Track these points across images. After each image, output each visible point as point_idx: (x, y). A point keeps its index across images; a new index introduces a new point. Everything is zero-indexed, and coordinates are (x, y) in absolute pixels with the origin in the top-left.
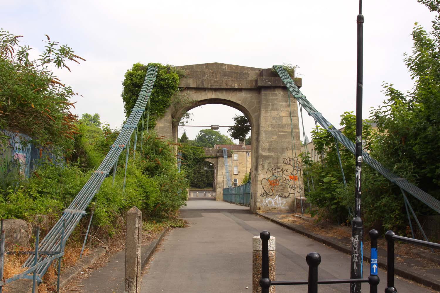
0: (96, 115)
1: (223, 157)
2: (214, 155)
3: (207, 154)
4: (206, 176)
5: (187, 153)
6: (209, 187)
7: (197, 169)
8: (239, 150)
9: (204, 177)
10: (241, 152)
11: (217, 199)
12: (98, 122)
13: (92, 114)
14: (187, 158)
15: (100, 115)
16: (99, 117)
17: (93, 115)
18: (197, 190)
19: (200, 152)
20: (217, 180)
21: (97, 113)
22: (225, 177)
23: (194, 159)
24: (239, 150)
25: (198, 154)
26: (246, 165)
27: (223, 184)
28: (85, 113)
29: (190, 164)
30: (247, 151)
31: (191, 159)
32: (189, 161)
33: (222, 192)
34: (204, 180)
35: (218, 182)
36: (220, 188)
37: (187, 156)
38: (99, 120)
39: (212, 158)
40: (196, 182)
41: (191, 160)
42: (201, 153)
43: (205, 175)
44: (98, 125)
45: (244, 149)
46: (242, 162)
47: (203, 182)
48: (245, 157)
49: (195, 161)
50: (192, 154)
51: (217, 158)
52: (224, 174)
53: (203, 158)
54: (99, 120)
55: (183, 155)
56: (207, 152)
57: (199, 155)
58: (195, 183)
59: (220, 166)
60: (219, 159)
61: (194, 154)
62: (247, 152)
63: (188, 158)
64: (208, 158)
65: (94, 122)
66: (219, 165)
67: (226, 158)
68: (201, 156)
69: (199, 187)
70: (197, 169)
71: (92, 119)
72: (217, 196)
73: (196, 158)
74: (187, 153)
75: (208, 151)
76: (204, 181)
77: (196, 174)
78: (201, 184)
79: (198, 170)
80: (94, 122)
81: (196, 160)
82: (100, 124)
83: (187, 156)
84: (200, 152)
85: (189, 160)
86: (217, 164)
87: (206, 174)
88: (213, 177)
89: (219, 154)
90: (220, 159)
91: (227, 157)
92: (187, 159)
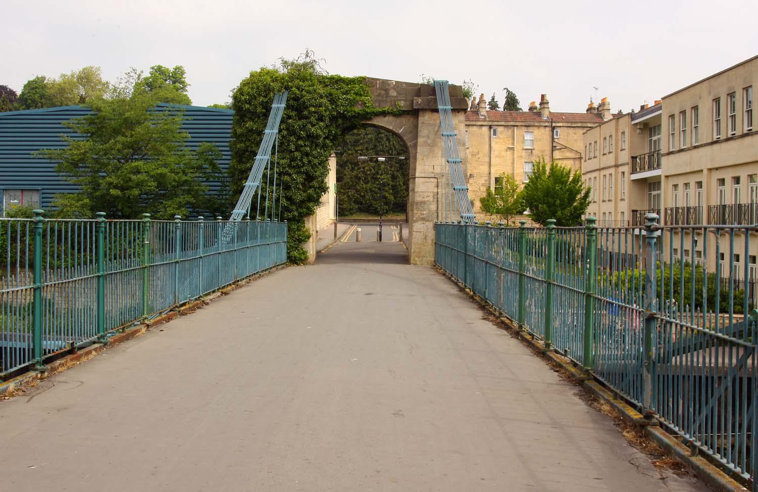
0: (179, 68)
1: (436, 111)
2: (402, 103)
3: (380, 102)
4: (392, 186)
5: (308, 96)
6: (398, 212)
7: (371, 170)
8: (474, 123)
9: (386, 188)
10: (475, 128)
11: (413, 258)
12: (183, 83)
13: (170, 66)
14: (306, 113)
15: (186, 69)
16: (183, 73)
17: (172, 70)
18: (370, 218)
19: (356, 94)
20: (414, 190)
21: (179, 65)
22: (443, 181)
23: (333, 119)
24: (474, 123)
25: (347, 99)
26: (487, 159)
27: (433, 207)
28: (156, 64)
29: (318, 137)
30: (490, 123)
31: (321, 119)
32: (313, 125)
33: (431, 234)
34: (387, 195)
35: (418, 199)
36: (423, 219)
37: (306, 108)
38: (184, 78)
39: (399, 114)
40: (369, 200)
41: (322, 121)
42: (358, 98)
43: (389, 185)
44: (182, 88)
45: (485, 120)
46: (478, 153)
47: (384, 200)
48: (487, 139)
49: (338, 126)
50: (324, 101)
51: (414, 113)
52: (438, 170)
53: (367, 116)
54: (184, 78)
55: (291, 102)
56: (379, 95)
57: (352, 103)
58: (366, 204)
59: (426, 144)
60: (421, 119)
61: (333, 101)
62: (490, 127)
63: (310, 112)
64: (384, 114)
65: (174, 82)
66: (421, 140)
67: (445, 111)
68: (358, 109)
69: (376, 212)
70: (371, 170)
71: (169, 76)
72: (414, 248)
73: (342, 116)
74: (308, 96)
75: (383, 92)
76: (385, 198)
77: (368, 182)
78: (377, 205)
79: (374, 174)
80: (174, 82)
81: (340, 121)
82: (185, 86)
83: (306, 108)
84: (356, 94)
85: (313, 119)
86: (416, 137)
87: (391, 183)
88: (407, 190)
89: (420, 100)
90: (425, 119)
91: (449, 107)
92: (307, 118)
